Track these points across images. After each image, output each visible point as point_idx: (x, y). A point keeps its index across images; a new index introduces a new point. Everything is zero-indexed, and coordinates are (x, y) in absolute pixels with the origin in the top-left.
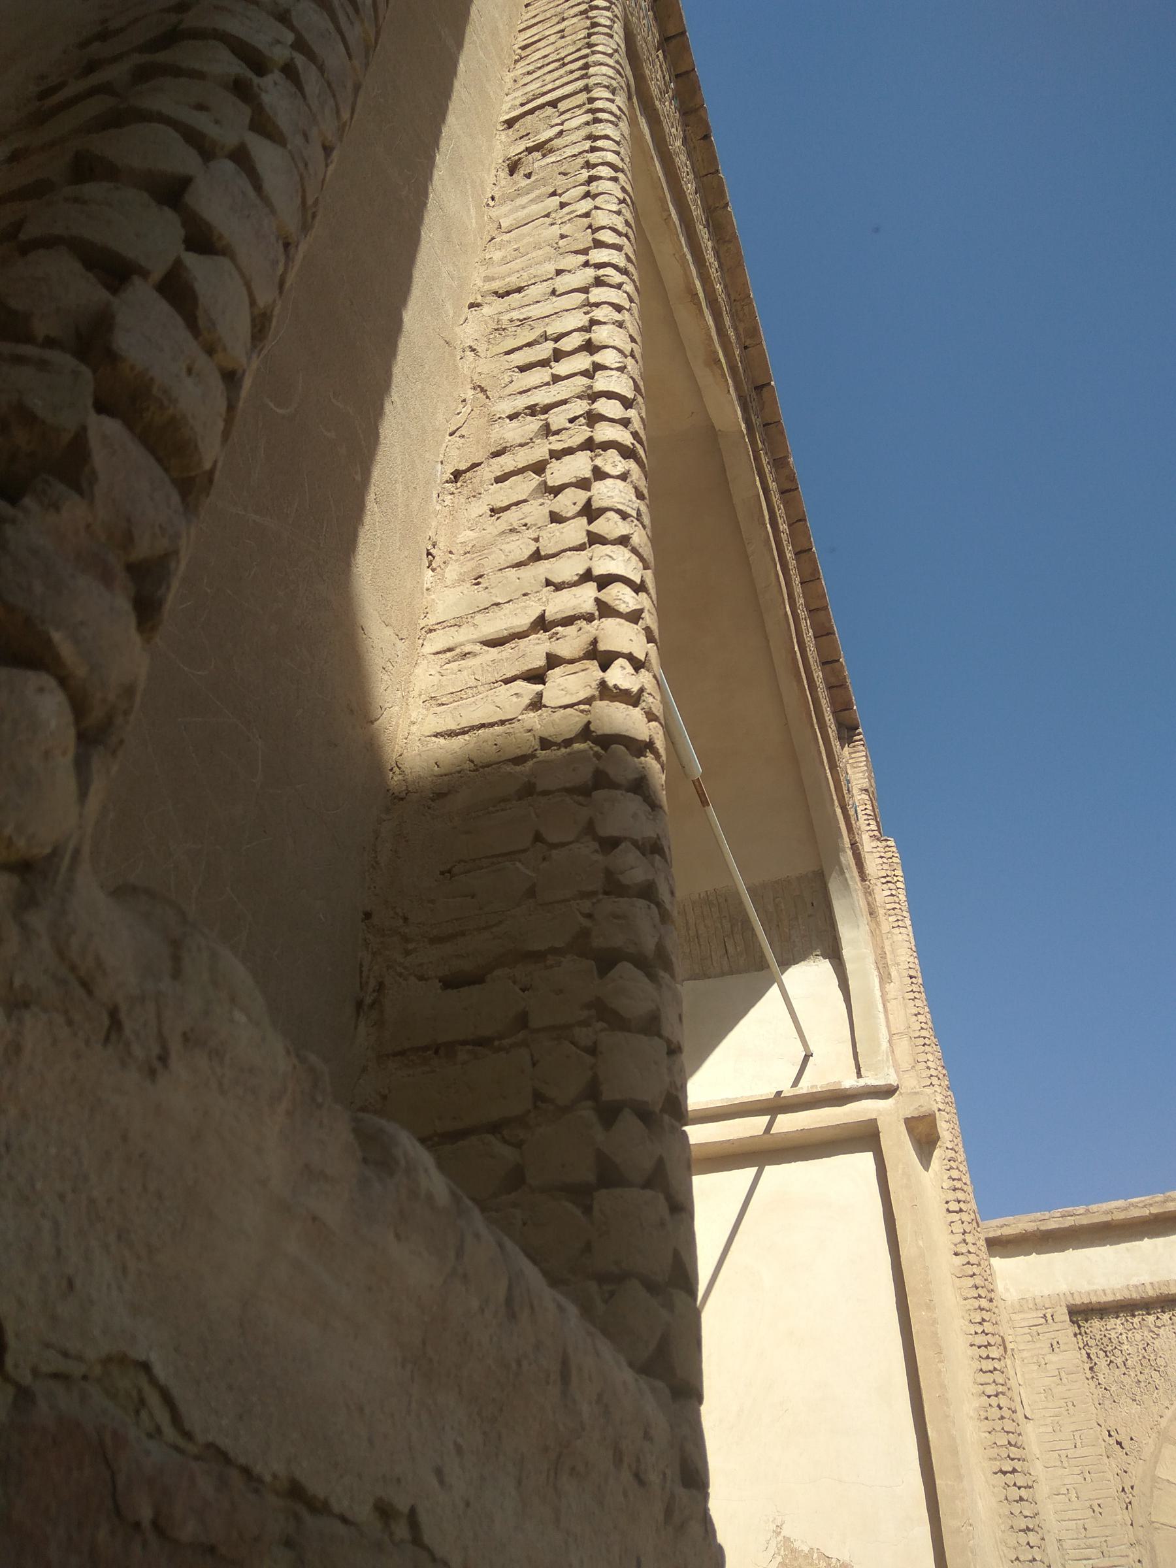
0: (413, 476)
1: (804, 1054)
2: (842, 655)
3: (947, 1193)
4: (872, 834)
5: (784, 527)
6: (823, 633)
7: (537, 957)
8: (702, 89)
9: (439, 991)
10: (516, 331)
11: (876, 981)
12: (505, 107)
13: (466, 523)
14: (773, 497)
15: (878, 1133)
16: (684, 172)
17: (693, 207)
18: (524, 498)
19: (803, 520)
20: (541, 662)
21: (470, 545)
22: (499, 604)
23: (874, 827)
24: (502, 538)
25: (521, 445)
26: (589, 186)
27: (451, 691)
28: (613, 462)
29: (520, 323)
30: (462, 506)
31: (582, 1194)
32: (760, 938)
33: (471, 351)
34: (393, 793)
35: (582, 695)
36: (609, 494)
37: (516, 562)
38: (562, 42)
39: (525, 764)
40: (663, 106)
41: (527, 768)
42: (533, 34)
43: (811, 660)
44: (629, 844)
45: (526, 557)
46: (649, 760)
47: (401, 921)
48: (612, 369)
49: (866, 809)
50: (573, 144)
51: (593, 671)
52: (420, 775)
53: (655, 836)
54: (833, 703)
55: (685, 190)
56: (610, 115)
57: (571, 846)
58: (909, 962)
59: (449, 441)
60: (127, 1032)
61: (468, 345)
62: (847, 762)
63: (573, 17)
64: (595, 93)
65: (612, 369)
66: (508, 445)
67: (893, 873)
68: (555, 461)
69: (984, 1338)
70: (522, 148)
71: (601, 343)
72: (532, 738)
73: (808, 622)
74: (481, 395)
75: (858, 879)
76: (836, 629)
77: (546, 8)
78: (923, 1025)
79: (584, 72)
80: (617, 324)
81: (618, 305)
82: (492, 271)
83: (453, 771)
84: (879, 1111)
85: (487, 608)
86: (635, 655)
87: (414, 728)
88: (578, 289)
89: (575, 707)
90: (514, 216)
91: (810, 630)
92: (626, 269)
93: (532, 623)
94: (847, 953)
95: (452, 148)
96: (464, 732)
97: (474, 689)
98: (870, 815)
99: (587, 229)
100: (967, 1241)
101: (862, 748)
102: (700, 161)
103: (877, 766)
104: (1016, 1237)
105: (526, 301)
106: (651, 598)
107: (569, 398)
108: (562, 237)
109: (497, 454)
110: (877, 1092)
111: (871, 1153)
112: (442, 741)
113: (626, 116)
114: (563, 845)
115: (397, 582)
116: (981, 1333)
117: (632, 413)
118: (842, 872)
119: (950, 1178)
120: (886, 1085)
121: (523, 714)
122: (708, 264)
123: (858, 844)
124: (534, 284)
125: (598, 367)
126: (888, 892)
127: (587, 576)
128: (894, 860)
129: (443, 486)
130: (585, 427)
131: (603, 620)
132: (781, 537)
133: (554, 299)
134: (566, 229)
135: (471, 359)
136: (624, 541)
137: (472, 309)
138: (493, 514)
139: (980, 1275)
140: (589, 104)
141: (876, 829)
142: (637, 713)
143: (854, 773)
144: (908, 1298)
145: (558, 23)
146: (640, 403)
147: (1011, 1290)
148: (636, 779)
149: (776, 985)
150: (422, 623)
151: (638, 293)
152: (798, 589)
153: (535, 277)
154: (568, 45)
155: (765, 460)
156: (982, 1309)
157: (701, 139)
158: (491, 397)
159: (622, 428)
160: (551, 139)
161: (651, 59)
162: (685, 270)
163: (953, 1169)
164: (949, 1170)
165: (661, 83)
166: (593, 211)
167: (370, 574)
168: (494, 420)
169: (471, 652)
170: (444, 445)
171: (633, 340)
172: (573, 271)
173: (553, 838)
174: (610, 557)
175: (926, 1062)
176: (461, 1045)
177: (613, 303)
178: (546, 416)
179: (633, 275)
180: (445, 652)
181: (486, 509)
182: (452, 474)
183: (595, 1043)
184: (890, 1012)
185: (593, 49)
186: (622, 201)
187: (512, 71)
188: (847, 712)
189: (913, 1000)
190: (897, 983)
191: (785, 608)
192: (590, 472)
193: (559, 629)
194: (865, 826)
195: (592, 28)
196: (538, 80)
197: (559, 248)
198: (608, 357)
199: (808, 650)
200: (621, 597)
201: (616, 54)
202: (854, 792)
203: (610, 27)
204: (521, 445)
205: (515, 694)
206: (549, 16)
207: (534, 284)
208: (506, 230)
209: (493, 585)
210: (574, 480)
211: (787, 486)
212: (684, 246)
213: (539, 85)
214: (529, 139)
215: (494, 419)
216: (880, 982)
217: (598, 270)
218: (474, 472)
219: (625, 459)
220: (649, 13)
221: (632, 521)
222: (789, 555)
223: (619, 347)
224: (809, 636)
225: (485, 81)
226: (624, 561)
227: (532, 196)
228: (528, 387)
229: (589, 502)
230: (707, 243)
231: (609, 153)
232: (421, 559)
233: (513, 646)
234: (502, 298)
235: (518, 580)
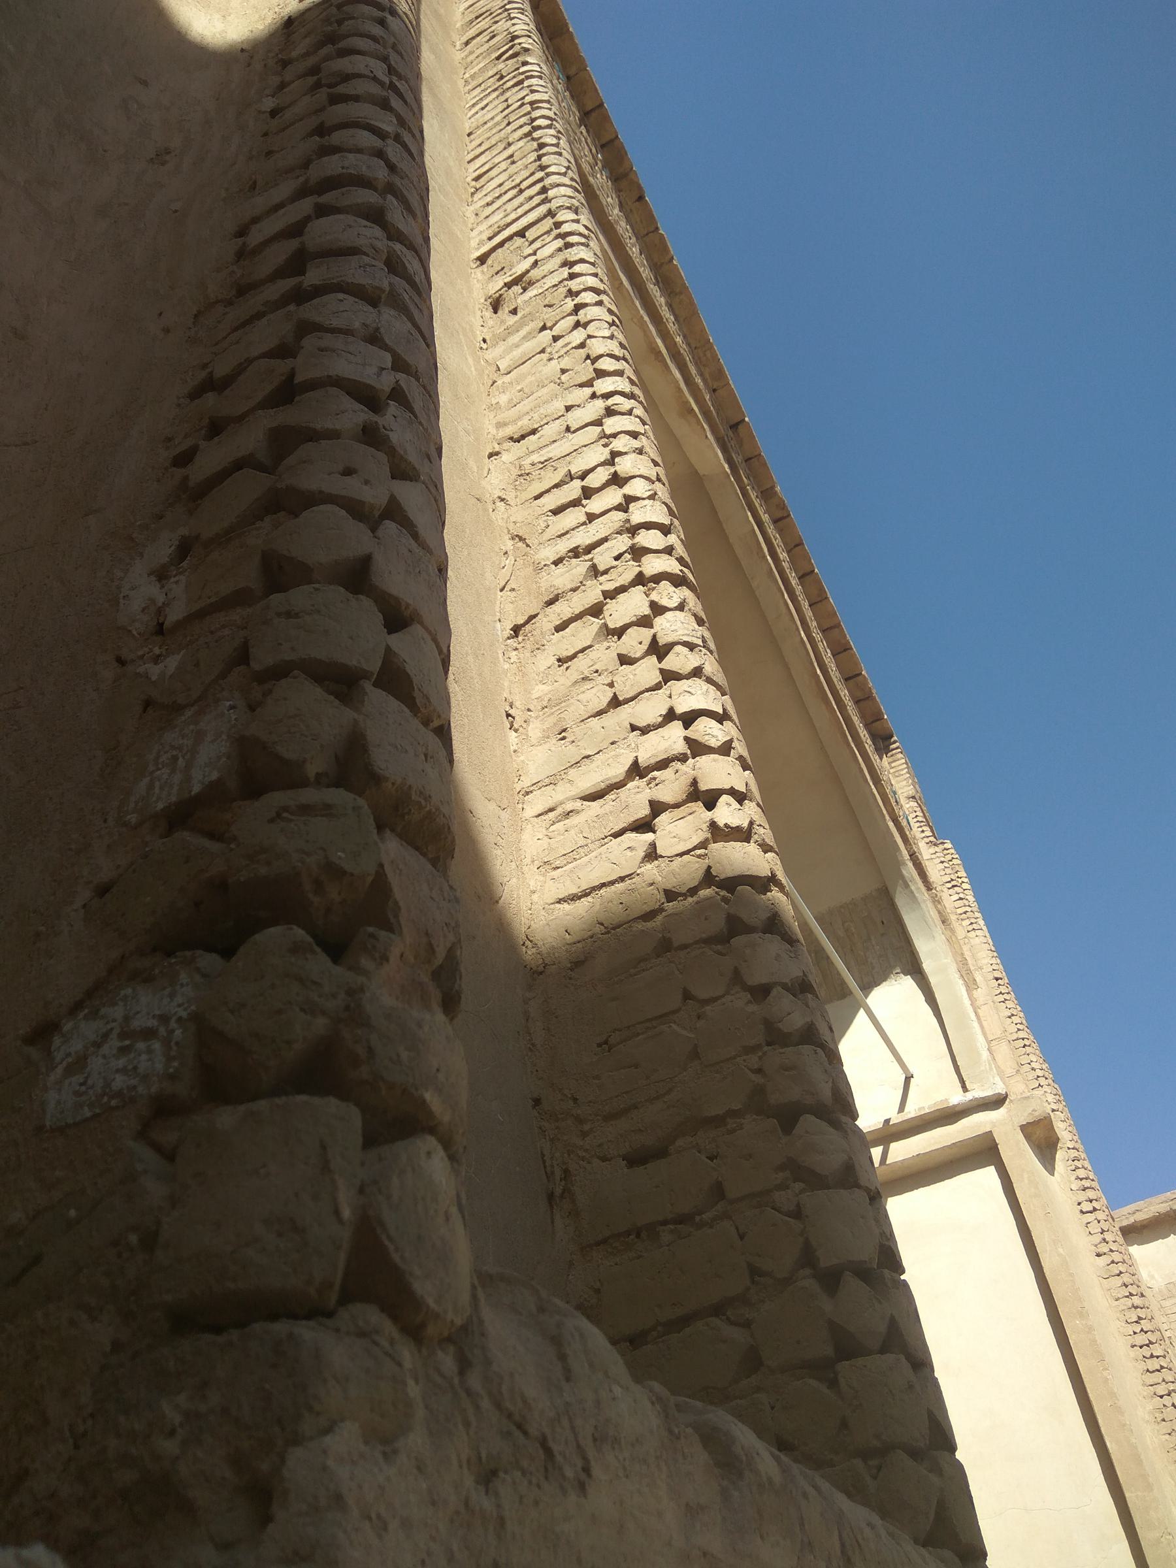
0: (479, 643)
1: (904, 1076)
2: (863, 668)
3: (1078, 1194)
4: (927, 840)
5: (783, 555)
6: (841, 650)
7: (718, 1121)
9: (626, 1170)
10: (540, 474)
11: (963, 990)
12: (474, 243)
13: (537, 678)
14: (768, 529)
15: (997, 1145)
16: (626, 238)
17: (641, 270)
18: (589, 644)
19: (800, 544)
20: (645, 811)
21: (546, 699)
22: (589, 756)
23: (929, 833)
25: (574, 590)
26: (577, 315)
28: (668, 595)
29: (542, 465)
30: (528, 660)
31: (824, 1370)
32: (836, 964)
34: (531, 968)
35: (696, 840)
36: (673, 628)
38: (513, 169)
39: (654, 920)
40: (596, 179)
41: (658, 923)
42: (482, 163)
43: (835, 680)
44: (779, 988)
45: (605, 705)
46: (775, 894)
47: (571, 1102)
48: (643, 499)
49: (917, 816)
50: (551, 274)
51: (699, 812)
52: (553, 945)
53: (802, 974)
54: (863, 717)
55: (631, 255)
56: (579, 237)
57: (723, 1000)
58: (991, 965)
60: (559, 1458)
61: (496, 496)
62: (889, 773)
63: (518, 140)
64: (560, 217)
65: (643, 499)
67: (957, 875)
68: (610, 601)
69: (1144, 1337)
70: (501, 284)
71: (627, 474)
72: (656, 892)
73: (824, 642)
74: (520, 544)
75: (923, 889)
76: (852, 644)
77: (489, 134)
78: (1019, 1026)
79: (543, 196)
80: (637, 451)
81: (634, 432)
82: (501, 417)
83: (586, 937)
84: (993, 1122)
85: (579, 762)
87: (535, 897)
88: (592, 422)
89: (691, 854)
90: (510, 356)
91: (828, 651)
92: (632, 393)
93: (627, 771)
94: (927, 966)
95: (440, 304)
96: (586, 894)
98: (922, 822)
99: (586, 359)
100: (1107, 1240)
101: (900, 756)
103: (918, 771)
104: (1150, 1221)
105: (543, 442)
106: (735, 724)
107: (609, 535)
108: (563, 371)
109: (550, 603)
110: (987, 1104)
111: (993, 1167)
112: (566, 905)
114: (714, 1000)
116: (1140, 1332)
117: (672, 539)
118: (907, 886)
119: (1078, 1178)
120: (994, 1094)
122: (665, 320)
123: (917, 854)
124: (547, 424)
125: (630, 499)
126: (956, 897)
127: (671, 716)
128: (955, 861)
130: (632, 563)
131: (698, 758)
132: (783, 566)
133: (570, 436)
134: (565, 363)
135: (503, 509)
136: (697, 672)
137: (491, 459)
138: (560, 664)
139: (1126, 1272)
140: (556, 229)
141: (931, 834)
142: (752, 848)
143: (898, 782)
144: (1059, 1309)
145: (505, 149)
146: (677, 526)
147: (1156, 1276)
148: (769, 918)
149: (862, 1010)
150: (518, 787)
151: (647, 413)
152: (809, 614)
153: (546, 416)
154: (521, 169)
155: (753, 495)
156: (1136, 1307)
157: (635, 202)
158: (531, 545)
159: (667, 556)
160: (528, 271)
161: (576, 138)
162: (644, 331)
163: (1079, 1168)
164: (1074, 1170)
165: (590, 159)
166: (588, 341)
168: (539, 568)
170: (498, 602)
171: (656, 464)
172: (582, 406)
173: (703, 995)
174: (689, 692)
175: (1029, 1064)
176: (661, 1225)
177: (629, 431)
178: (590, 556)
179: (639, 397)
180: (546, 812)
181: (553, 660)
182: (511, 630)
183: (798, 1205)
184: (982, 1019)
185: (548, 170)
186: (613, 324)
187: (471, 205)
188: (878, 722)
189: (1003, 1002)
190: (984, 988)
191: (800, 634)
192: (648, 609)
193: (655, 773)
194: (920, 834)
195: (540, 150)
196: (499, 211)
197: (563, 383)
198: (637, 488)
199: (830, 670)
200: (709, 731)
201: (570, 171)
202: (902, 802)
203: (557, 145)
204: (574, 590)
206: (494, 143)
207: (547, 424)
208: (506, 372)
209: (579, 738)
210: (634, 619)
211: (779, 514)
212: (640, 308)
213: (501, 215)
214: (505, 273)
215: (540, 568)
216: (967, 990)
217: (607, 400)
218: (533, 624)
219: (676, 587)
220: (566, 94)
221: (700, 651)
222: (794, 582)
223: (645, 475)
224: (828, 657)
225: (450, 223)
226: (703, 693)
227: (523, 332)
228: (566, 530)
229: (654, 638)
230: (660, 300)
231: (588, 277)
232: (503, 723)
233: (613, 797)
234: (519, 442)
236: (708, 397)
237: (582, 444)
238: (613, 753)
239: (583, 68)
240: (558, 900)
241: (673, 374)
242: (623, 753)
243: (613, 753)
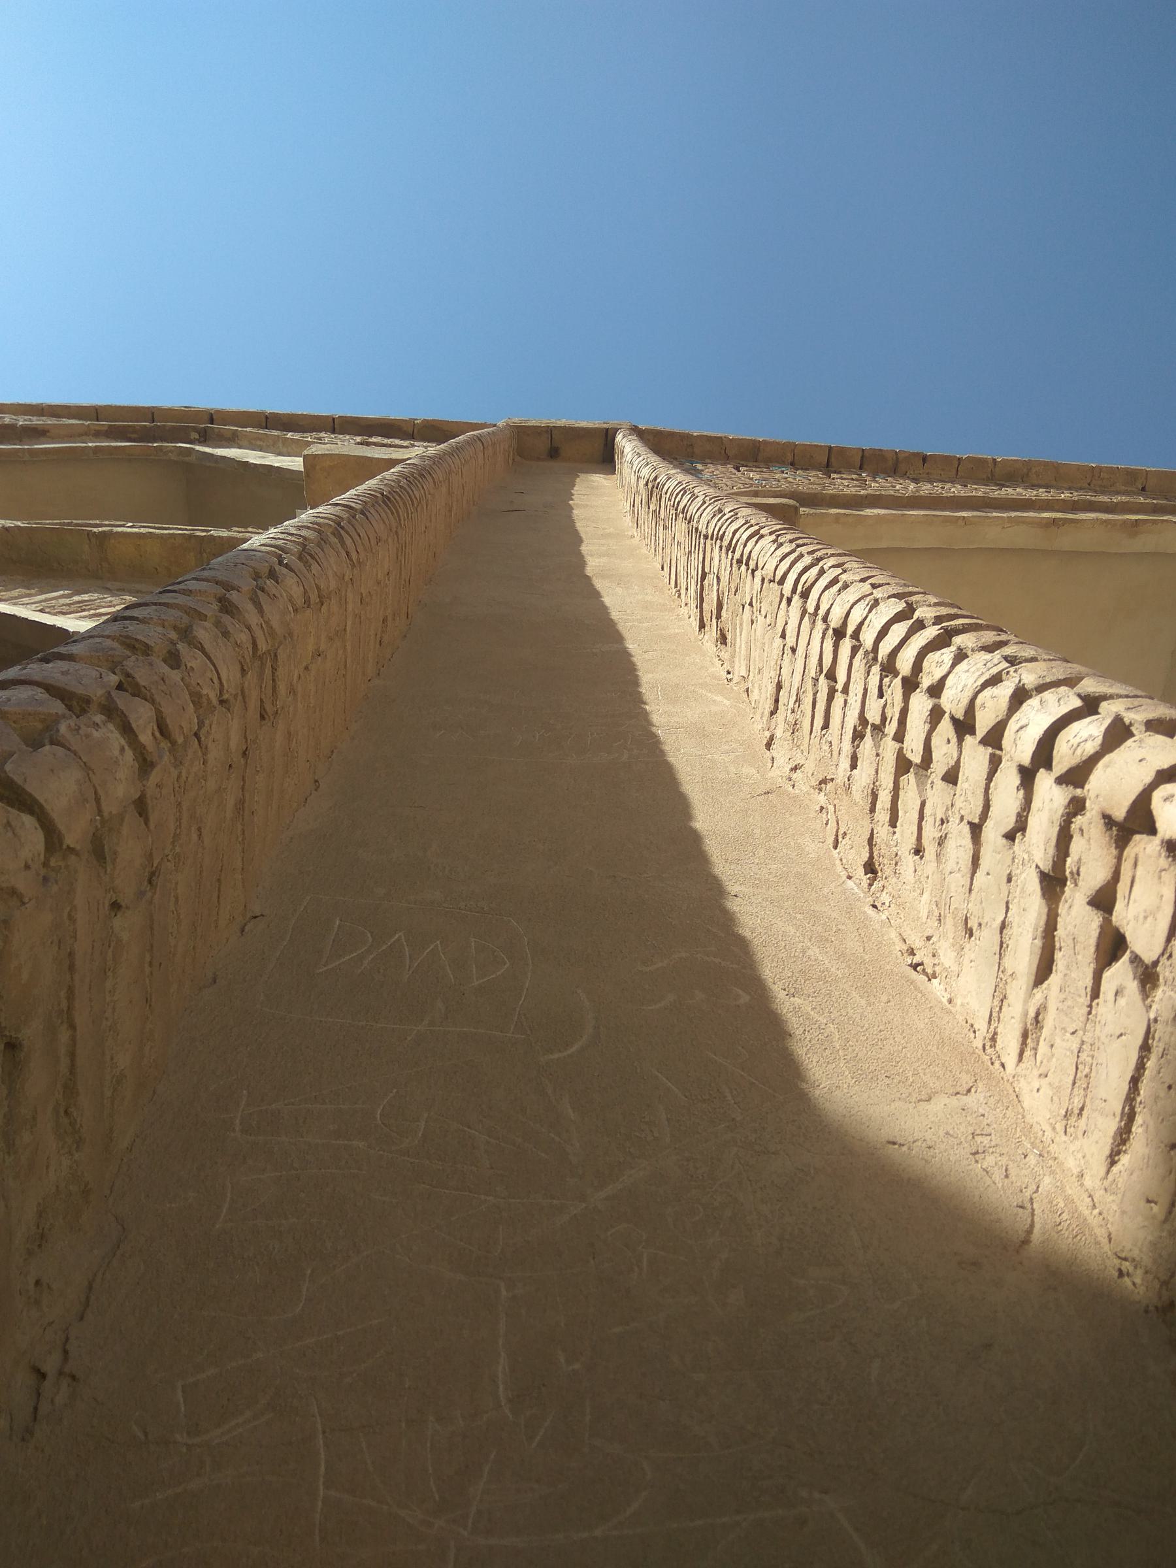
8: (882, 449)
20: (1095, 920)
24: (944, 861)
27: (1071, 1082)
29: (798, 703)
33: (795, 772)
36: (960, 689)
37: (970, 863)
48: (867, 617)
59: (839, 853)
66: (872, 786)
87: (1088, 1182)
96: (1129, 1117)
97: (1084, 1047)
102: (942, 473)
112: (1125, 1160)
113: (740, 508)
115: (899, 1038)
121: (1151, 1007)
124: (781, 668)
127: (1027, 776)
129: (871, 894)
150: (978, 1043)
153: (776, 664)
167: (847, 1073)
169: (1039, 1009)
170: (838, 862)
174: (1022, 728)
177: (826, 587)
182: (866, 874)
205: (1116, 995)
207: (781, 668)
209: (980, 914)
210: (927, 726)
223: (856, 599)
235: (989, 877)
236: (1142, 499)
237: (806, 645)
238: (1018, 890)
240: (1109, 1160)
241: (1086, 520)
242: (1025, 878)
243: (1018, 890)
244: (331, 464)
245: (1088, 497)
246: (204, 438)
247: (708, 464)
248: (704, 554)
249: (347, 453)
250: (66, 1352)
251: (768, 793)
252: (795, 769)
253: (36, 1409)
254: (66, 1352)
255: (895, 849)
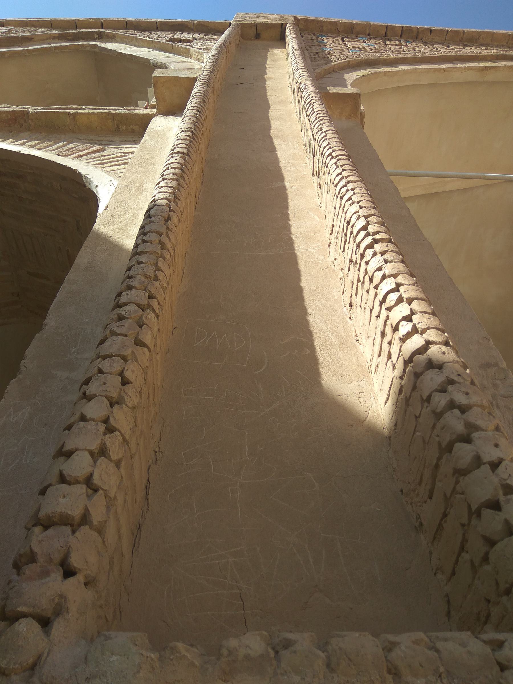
59: (343, 297)
86: (405, 315)
96: (389, 395)
112: (387, 404)
150: (367, 366)
162: (471, 69)
239: (369, 26)
241: (500, 66)
244: (164, 81)
245: (504, 52)
246: (101, 37)
247: (329, 37)
248: (315, 146)
249: (170, 75)
250: (159, 447)
251: (326, 268)
252: (336, 259)
253: (156, 458)
254: (159, 447)
255: (356, 303)
